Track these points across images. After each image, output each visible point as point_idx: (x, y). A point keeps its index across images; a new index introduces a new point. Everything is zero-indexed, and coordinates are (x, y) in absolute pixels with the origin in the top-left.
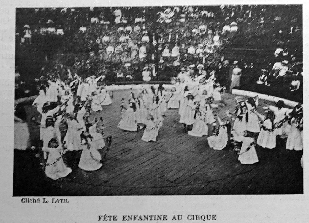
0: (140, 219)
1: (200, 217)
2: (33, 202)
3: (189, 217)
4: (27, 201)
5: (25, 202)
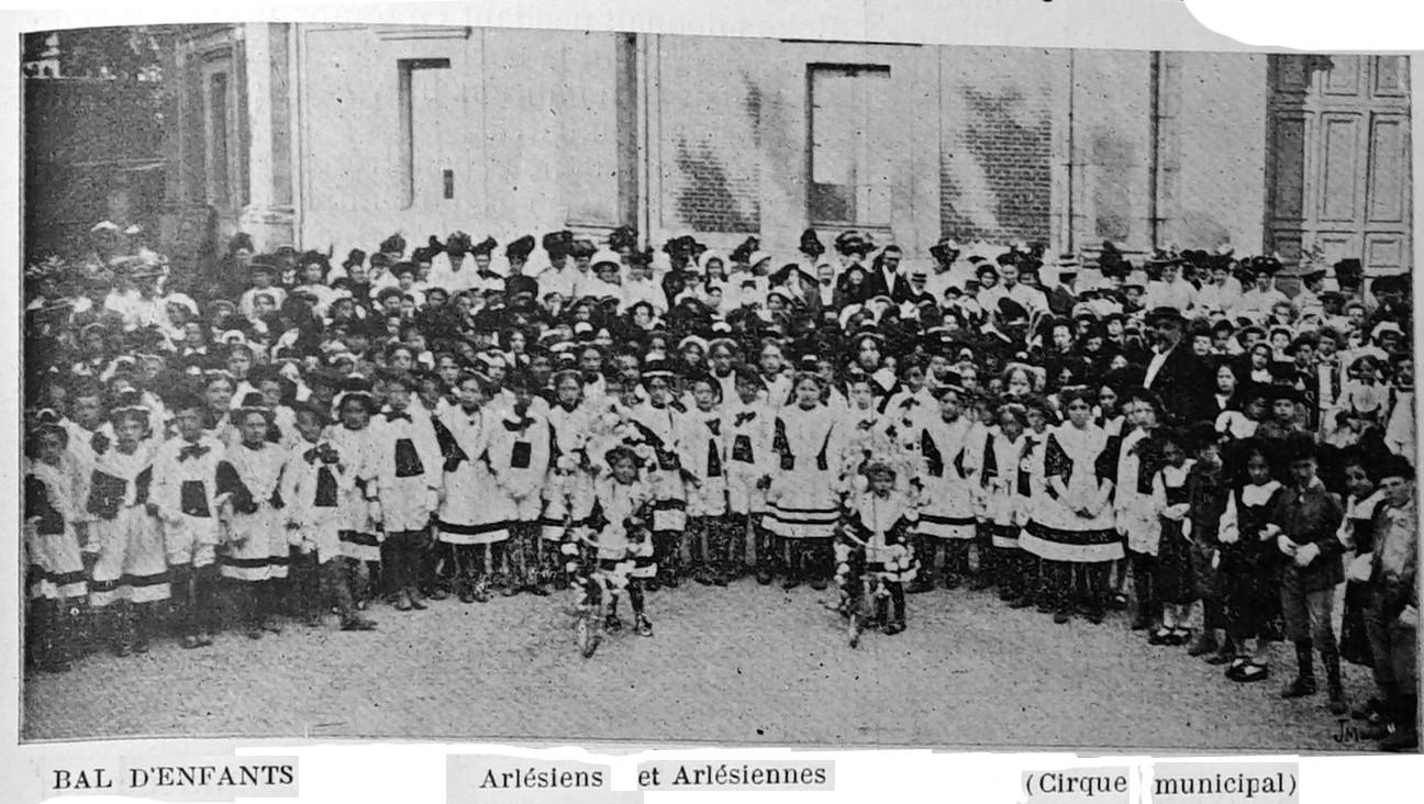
0: (489, 784)
3: (1048, 778)
5: (1054, 789)
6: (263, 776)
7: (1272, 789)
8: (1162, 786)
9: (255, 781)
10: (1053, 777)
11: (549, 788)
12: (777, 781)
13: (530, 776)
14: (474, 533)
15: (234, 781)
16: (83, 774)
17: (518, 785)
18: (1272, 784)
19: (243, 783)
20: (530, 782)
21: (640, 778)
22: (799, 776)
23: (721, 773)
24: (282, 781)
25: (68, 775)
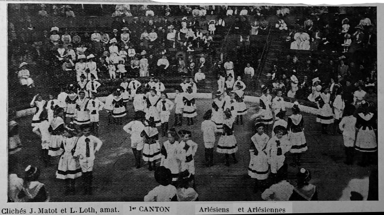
3: (4, 210)
4: (9, 212)
5: (5, 213)
6: (155, 209)
7: (103, 211)
8: (102, 210)
9: (169, 211)
10: (5, 209)
11: (104, 212)
12: (109, 211)
13: (21, 211)
14: (121, 115)
15: (148, 210)
16: (146, 208)
17: (208, 211)
18: (103, 210)
19: (150, 211)
20: (211, 211)
21: (61, 211)
22: (279, 210)
23: (211, 209)
25: (101, 211)
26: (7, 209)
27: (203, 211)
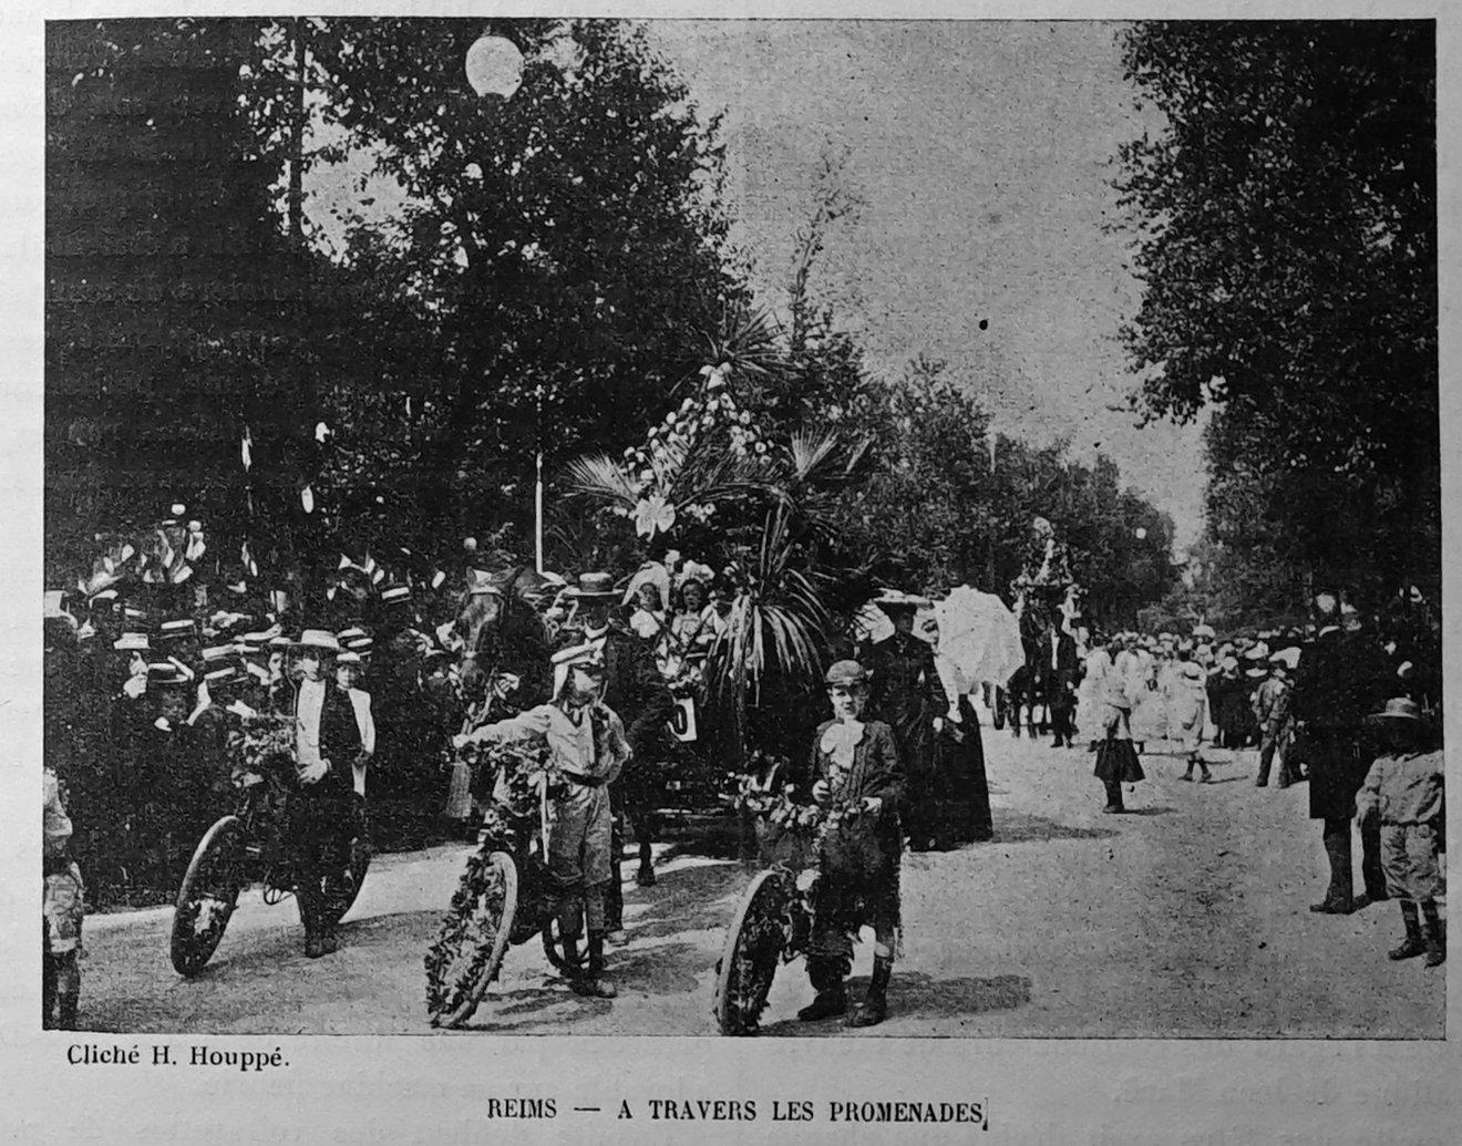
1: (859, 1112)
2: (116, 1061)
24: (746, 1117)
26: (87, 1047)
27: (691, 1117)
